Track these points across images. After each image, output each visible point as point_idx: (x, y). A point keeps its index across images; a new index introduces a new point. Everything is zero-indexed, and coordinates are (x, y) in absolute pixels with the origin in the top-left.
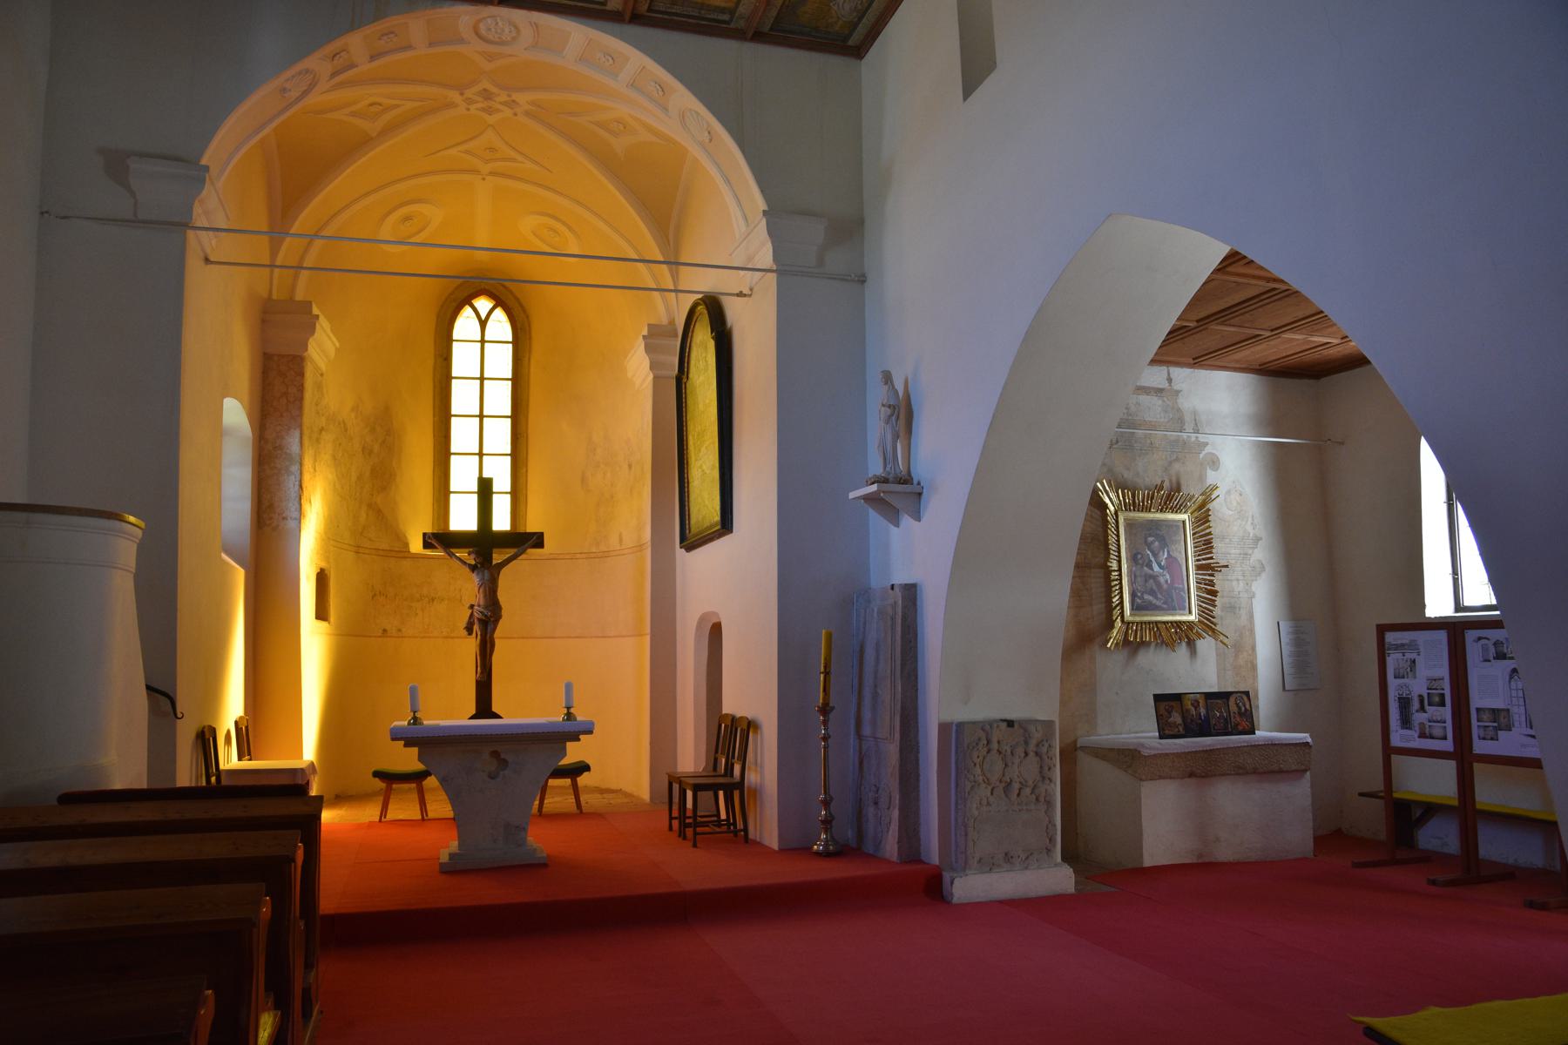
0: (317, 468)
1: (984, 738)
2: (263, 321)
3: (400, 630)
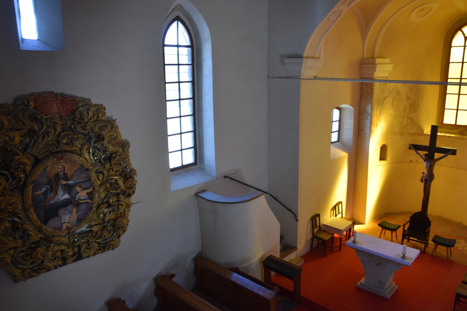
0: (382, 113)
3: (417, 160)
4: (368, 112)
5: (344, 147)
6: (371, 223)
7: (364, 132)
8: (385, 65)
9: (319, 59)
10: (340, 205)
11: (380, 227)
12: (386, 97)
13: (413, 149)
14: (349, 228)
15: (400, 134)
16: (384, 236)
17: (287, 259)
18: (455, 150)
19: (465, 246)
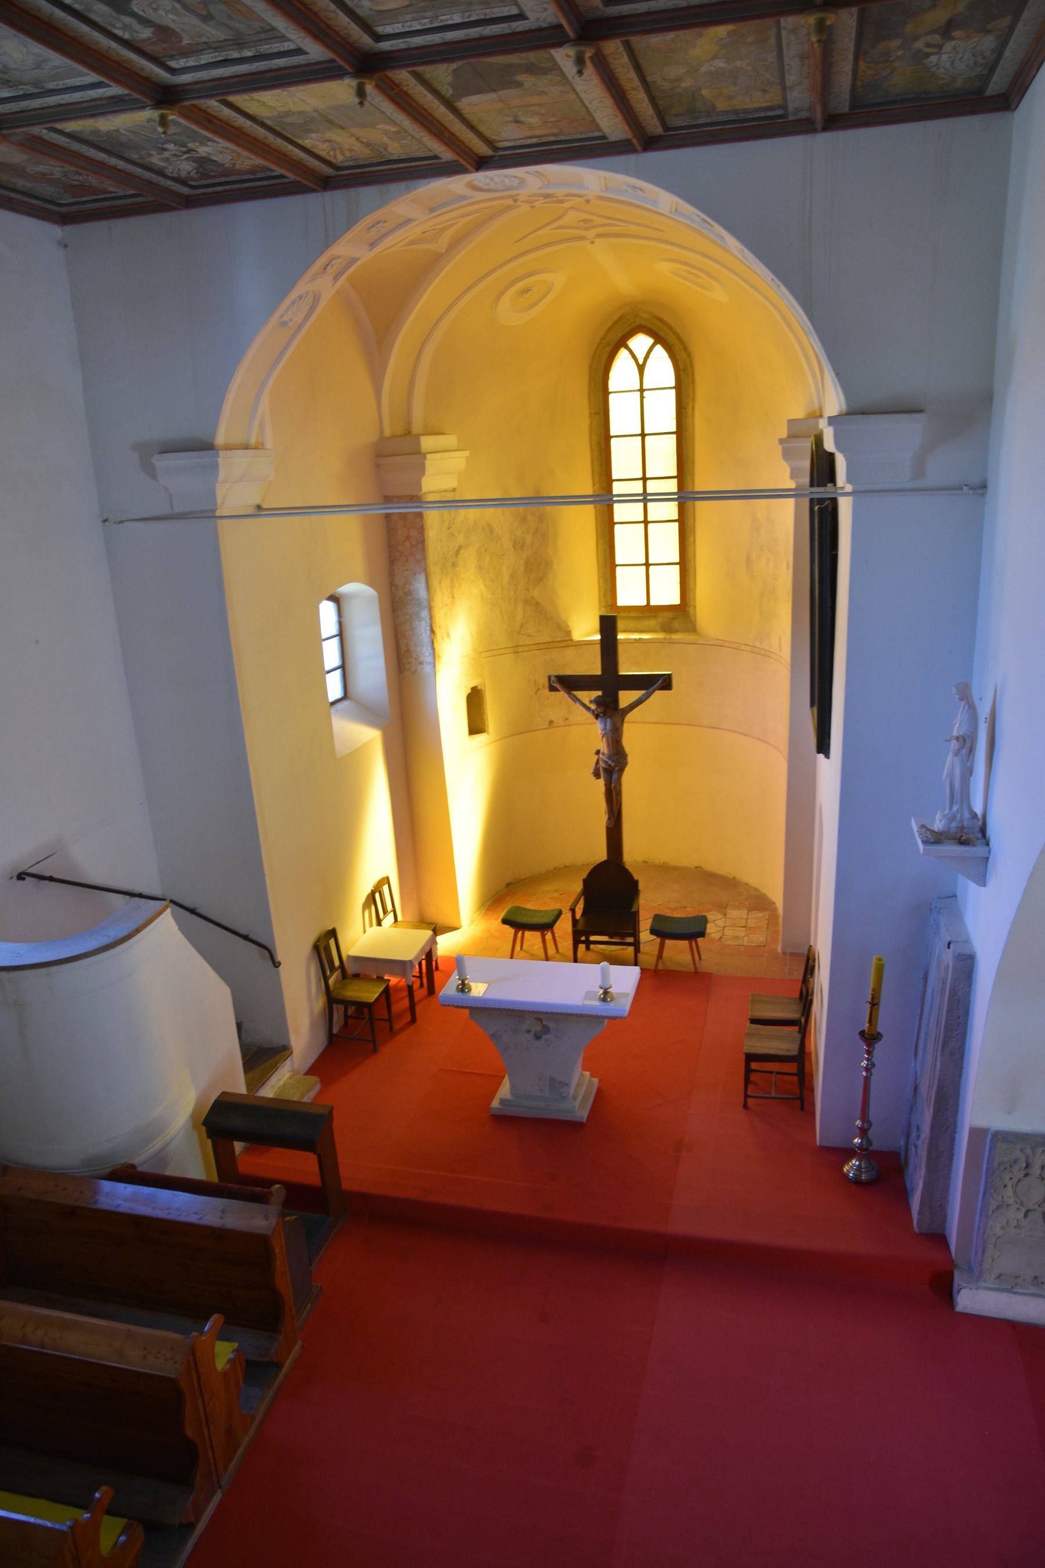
0: (455, 595)
1: (1023, 1159)
2: (378, 466)
3: (567, 719)
4: (419, 600)
5: (368, 714)
6: (475, 923)
7: (416, 659)
8: (438, 455)
9: (263, 449)
10: (385, 888)
11: (507, 927)
12: (460, 547)
13: (560, 689)
14: (427, 950)
15: (510, 650)
16: (521, 949)
17: (268, 1091)
18: (669, 676)
19: (725, 926)
